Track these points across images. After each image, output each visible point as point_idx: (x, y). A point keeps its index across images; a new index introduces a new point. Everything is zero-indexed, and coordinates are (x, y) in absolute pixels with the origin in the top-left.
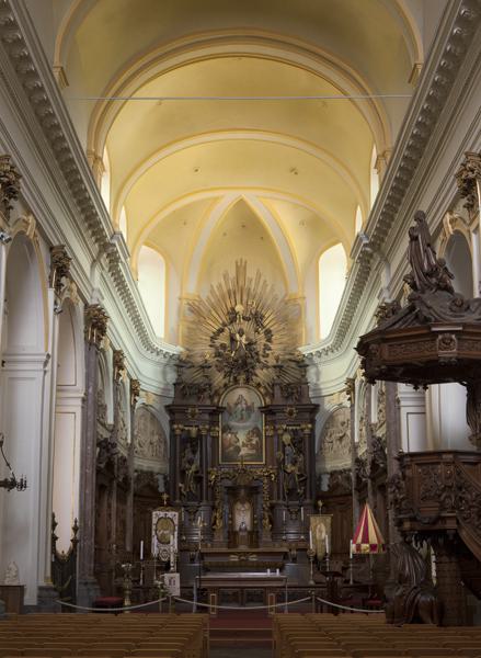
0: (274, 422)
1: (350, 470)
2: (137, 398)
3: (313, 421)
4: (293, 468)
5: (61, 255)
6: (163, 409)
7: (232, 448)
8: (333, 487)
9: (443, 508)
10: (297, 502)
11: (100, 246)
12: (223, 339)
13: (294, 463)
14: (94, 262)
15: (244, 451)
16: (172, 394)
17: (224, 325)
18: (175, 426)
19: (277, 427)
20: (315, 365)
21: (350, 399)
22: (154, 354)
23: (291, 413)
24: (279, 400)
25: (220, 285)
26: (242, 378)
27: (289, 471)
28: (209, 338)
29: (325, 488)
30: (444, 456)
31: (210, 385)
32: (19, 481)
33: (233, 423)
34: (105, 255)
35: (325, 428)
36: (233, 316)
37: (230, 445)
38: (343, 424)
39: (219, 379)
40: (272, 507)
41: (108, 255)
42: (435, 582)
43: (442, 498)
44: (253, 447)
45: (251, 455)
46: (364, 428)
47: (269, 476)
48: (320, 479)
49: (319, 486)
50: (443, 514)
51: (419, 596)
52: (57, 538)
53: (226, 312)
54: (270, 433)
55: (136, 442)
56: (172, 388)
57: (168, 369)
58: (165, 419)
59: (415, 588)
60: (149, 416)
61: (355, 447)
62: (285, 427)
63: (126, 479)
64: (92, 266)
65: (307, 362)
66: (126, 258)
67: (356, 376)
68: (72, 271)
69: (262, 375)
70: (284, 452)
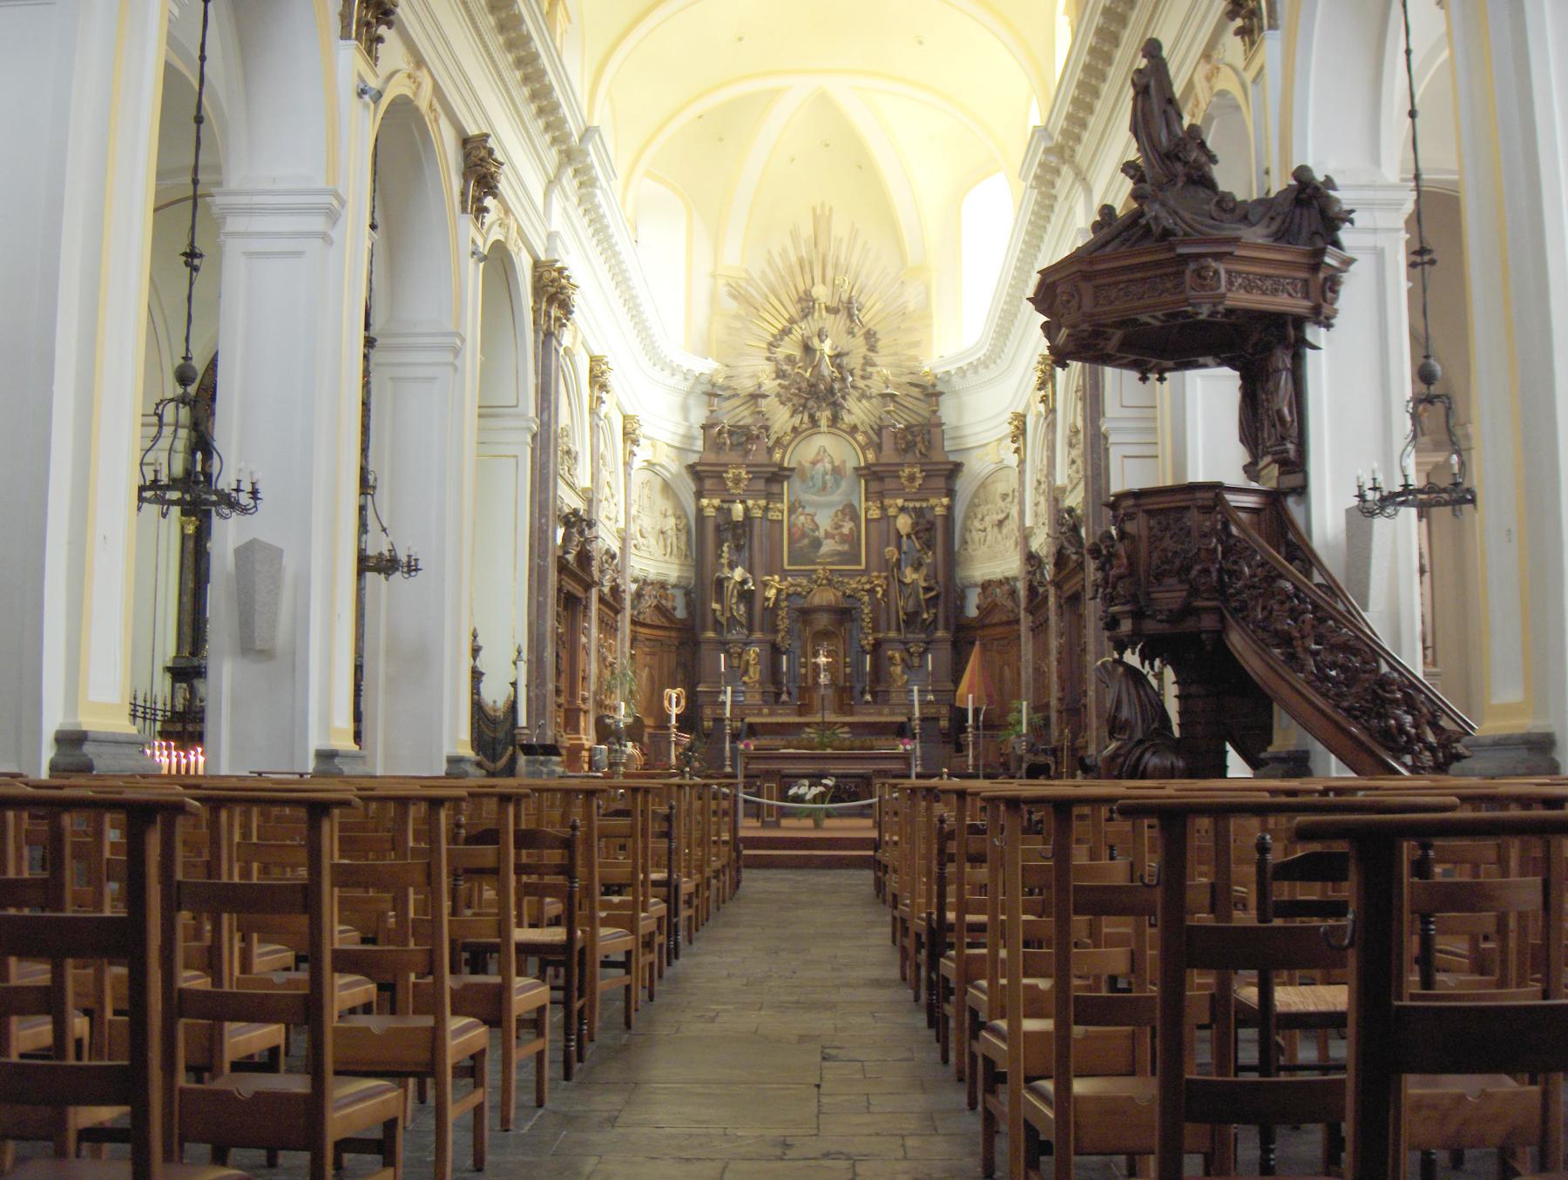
0: (881, 495)
1: (1015, 579)
2: (604, 395)
3: (951, 493)
4: (915, 576)
5: (555, 274)
6: (684, 472)
7: (806, 541)
8: (986, 610)
9: (1194, 592)
10: (923, 636)
11: (560, 152)
12: (790, 348)
13: (917, 566)
14: (551, 184)
15: (828, 546)
16: (699, 445)
17: (792, 321)
18: (705, 502)
19: (887, 502)
20: (956, 393)
21: (1017, 451)
22: (668, 372)
23: (912, 478)
24: (889, 455)
25: (784, 250)
26: (824, 416)
27: (908, 580)
28: (765, 346)
29: (972, 612)
30: (1198, 495)
31: (767, 428)
32: (404, 559)
33: (808, 497)
34: (570, 171)
35: (967, 517)
36: (807, 306)
37: (804, 535)
38: (1005, 496)
39: (782, 418)
40: (877, 645)
41: (576, 171)
42: (1176, 732)
43: (1194, 573)
44: (844, 539)
45: (840, 553)
46: (1042, 499)
47: (872, 591)
48: (962, 597)
49: (961, 608)
50: (1199, 603)
51: (1147, 756)
52: (482, 674)
53: (795, 297)
54: (875, 513)
55: (634, 529)
56: (699, 433)
57: (692, 401)
58: (687, 487)
59: (1140, 742)
60: (658, 483)
61: (1026, 536)
62: (900, 502)
63: (615, 590)
64: (547, 194)
65: (939, 388)
66: (608, 180)
67: (1028, 406)
68: (503, 186)
69: (857, 412)
70: (899, 547)
